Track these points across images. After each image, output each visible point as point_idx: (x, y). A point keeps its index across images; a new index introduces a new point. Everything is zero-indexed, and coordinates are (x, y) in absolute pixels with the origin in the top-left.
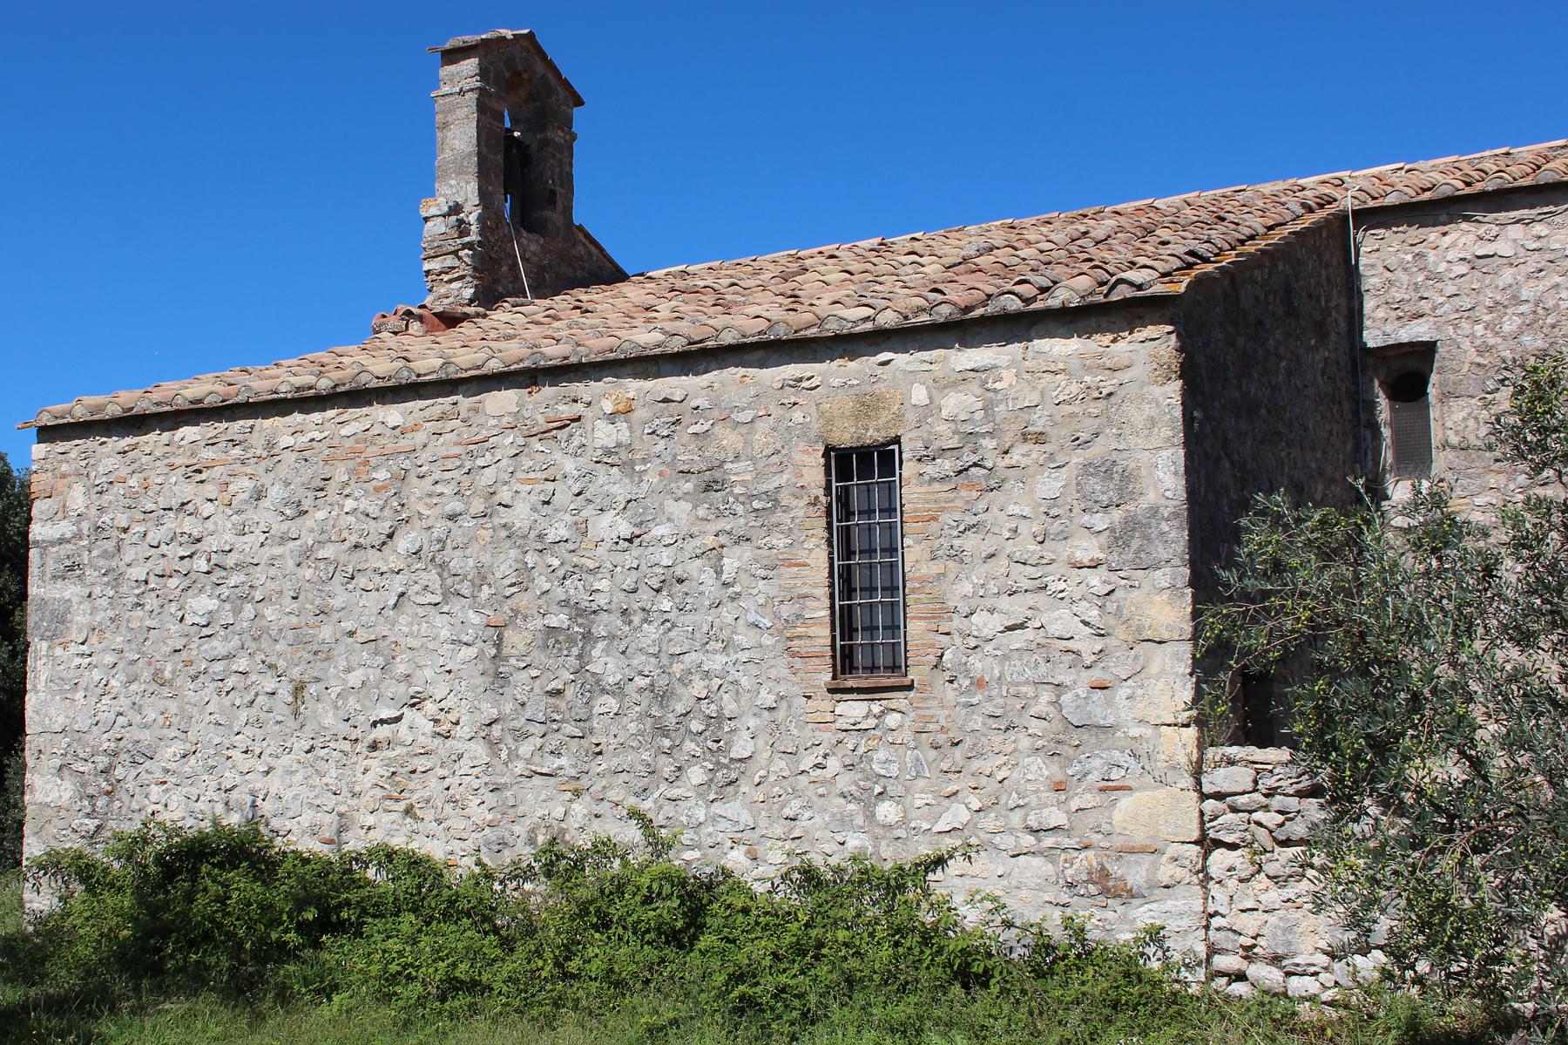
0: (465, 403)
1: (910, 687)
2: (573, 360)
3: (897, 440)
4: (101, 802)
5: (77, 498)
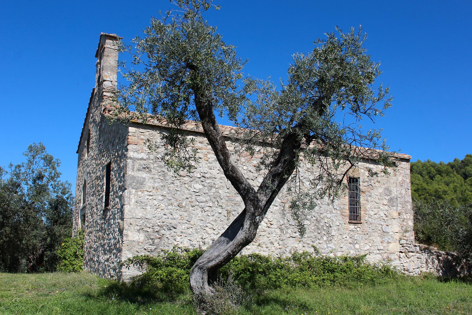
1: (361, 223)
3: (359, 178)
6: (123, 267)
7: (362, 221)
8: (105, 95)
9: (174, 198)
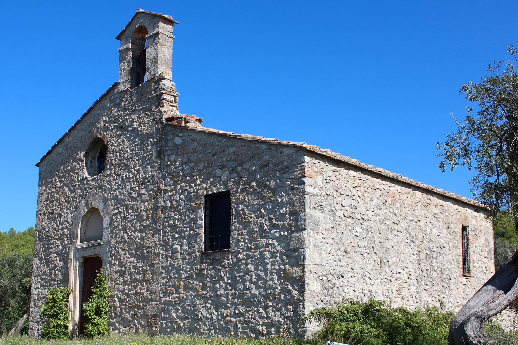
0: (412, 192)
1: (470, 277)
2: (434, 190)
3: (468, 227)
4: (330, 291)
5: (319, 181)
6: (307, 321)
7: (471, 274)
8: (165, 99)
9: (341, 241)
